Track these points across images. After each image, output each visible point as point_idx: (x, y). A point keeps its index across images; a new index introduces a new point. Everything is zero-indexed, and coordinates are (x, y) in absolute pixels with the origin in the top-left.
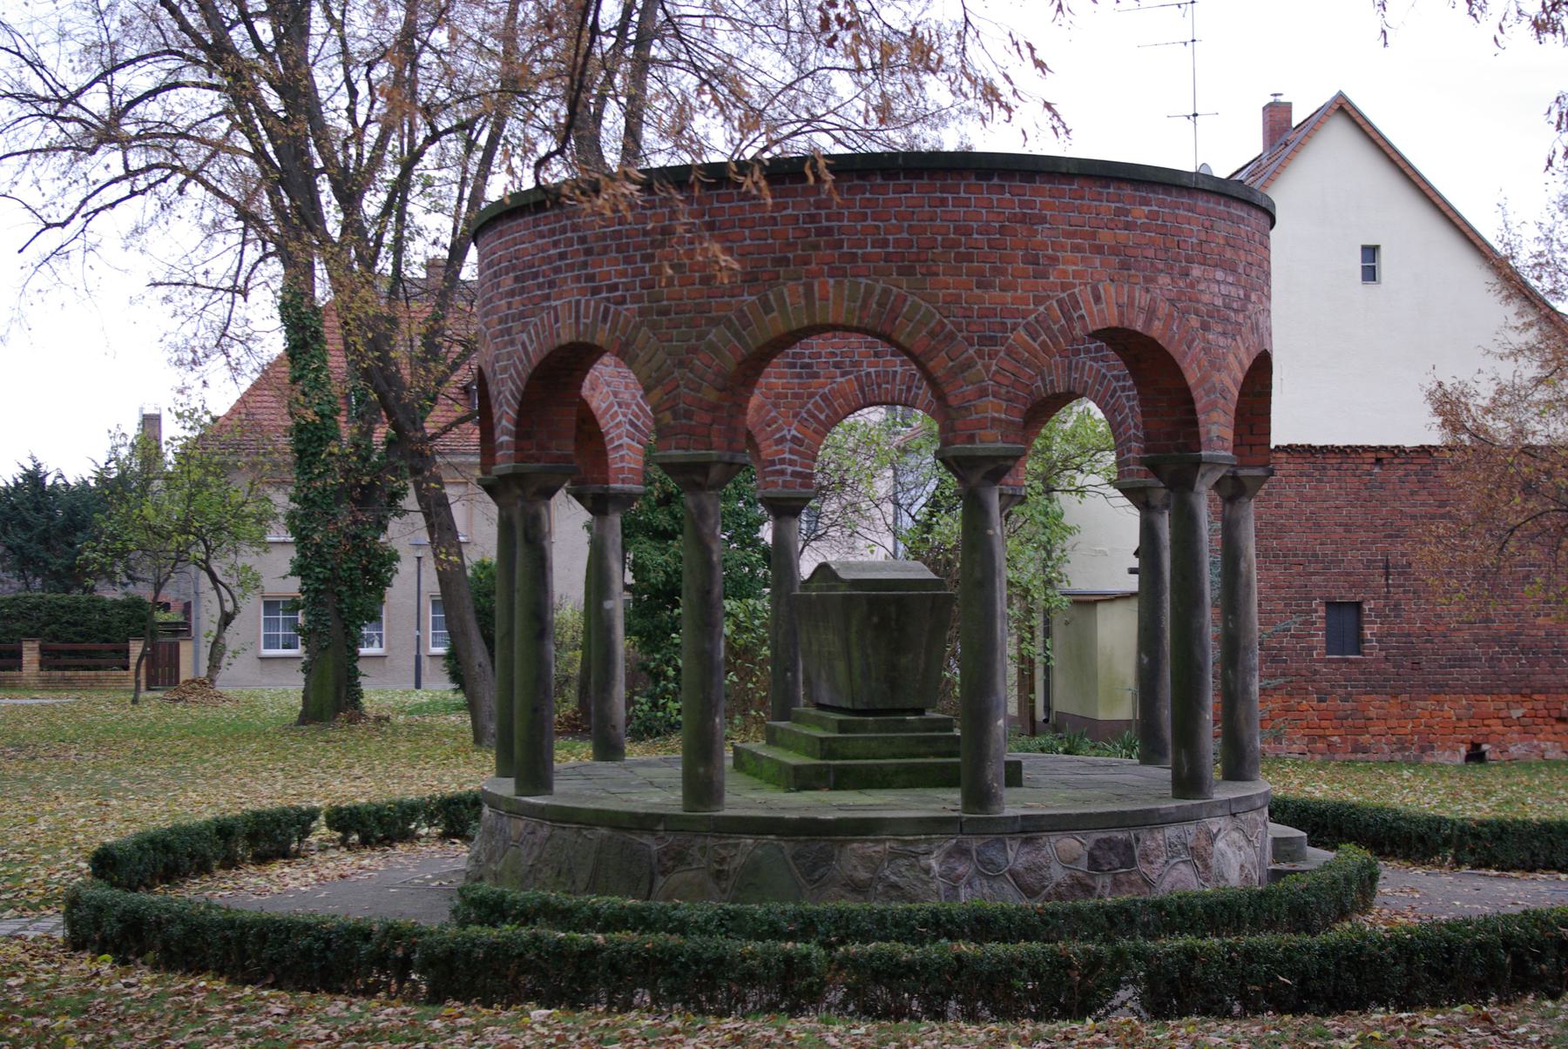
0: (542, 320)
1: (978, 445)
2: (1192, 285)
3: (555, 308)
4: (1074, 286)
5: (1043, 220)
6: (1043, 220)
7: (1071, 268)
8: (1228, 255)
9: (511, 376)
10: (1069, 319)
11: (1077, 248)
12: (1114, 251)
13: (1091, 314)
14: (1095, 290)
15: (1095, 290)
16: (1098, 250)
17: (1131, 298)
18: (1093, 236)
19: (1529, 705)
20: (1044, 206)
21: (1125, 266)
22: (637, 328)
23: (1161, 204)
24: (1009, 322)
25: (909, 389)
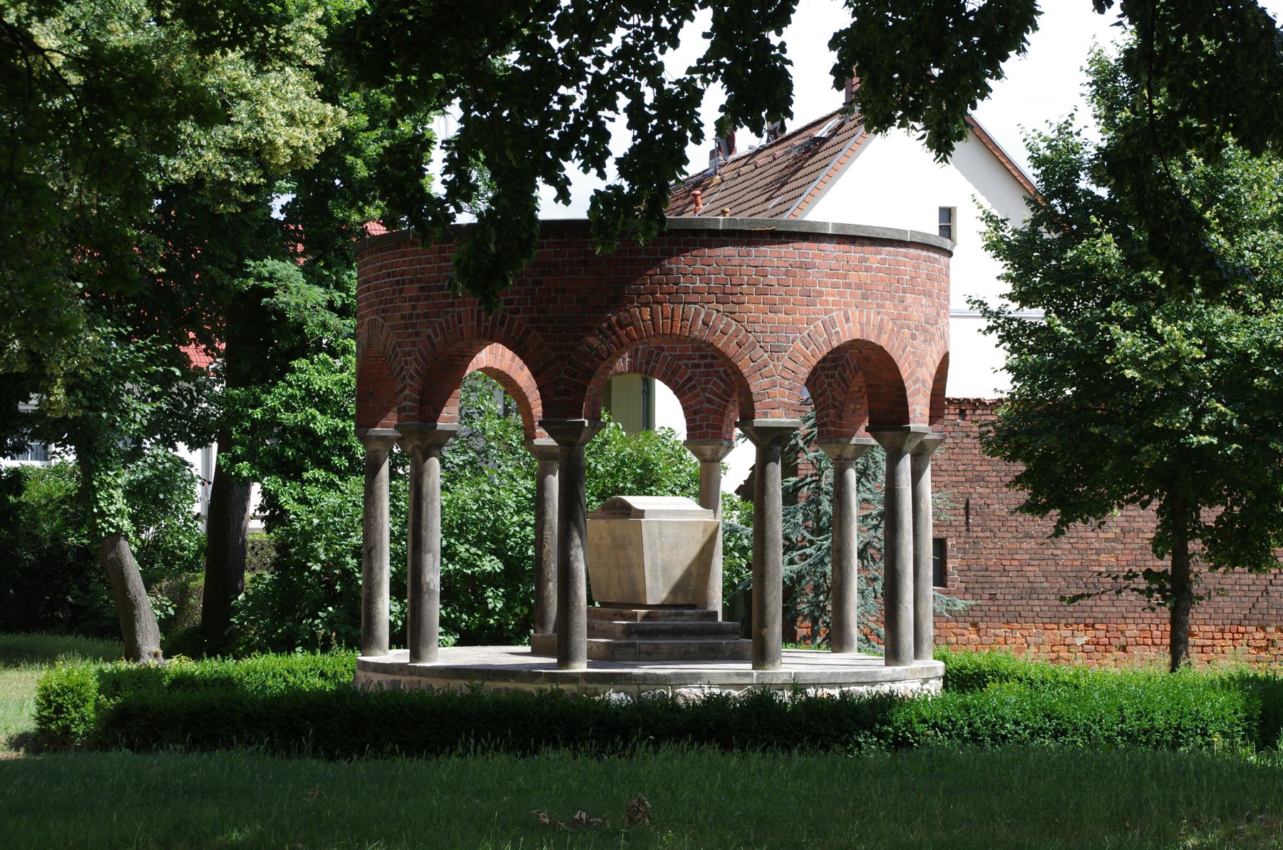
0: (446, 321)
1: (770, 420)
2: (906, 309)
3: (459, 314)
4: (832, 311)
5: (813, 266)
6: (813, 266)
7: (831, 299)
8: (928, 286)
9: (416, 359)
10: (829, 334)
11: (835, 286)
12: (859, 287)
13: (843, 330)
14: (846, 313)
15: (846, 313)
16: (848, 286)
17: (868, 318)
18: (845, 277)
19: (1091, 633)
20: (815, 256)
21: (865, 297)
22: (527, 332)
23: (889, 254)
24: (791, 336)
25: (648, 363)
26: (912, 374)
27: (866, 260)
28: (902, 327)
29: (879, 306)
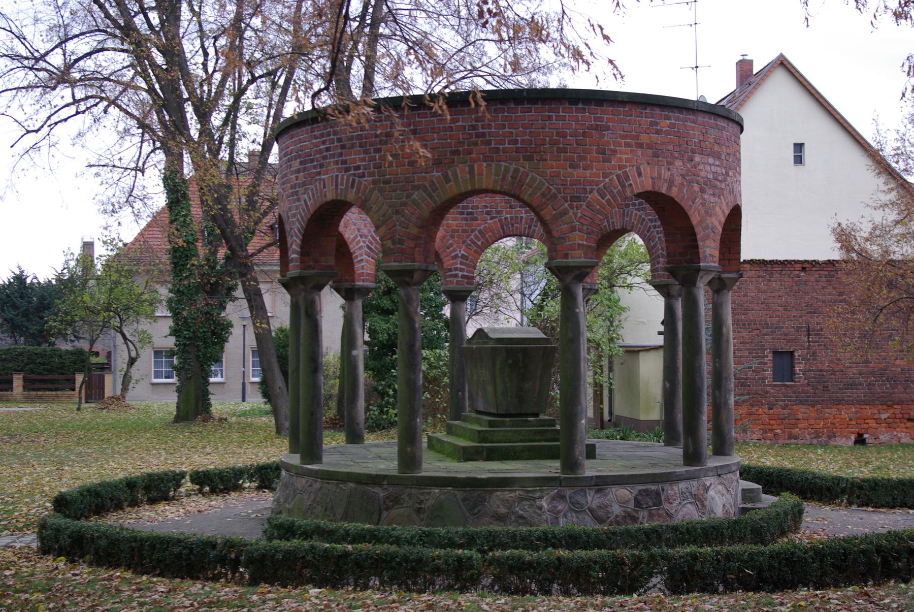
0: (316, 186)
1: (570, 260)
2: (695, 166)
3: (324, 180)
4: (626, 167)
5: (608, 128)
6: (608, 128)
7: (624, 156)
9: (298, 220)
10: (623, 186)
11: (628, 145)
12: (650, 146)
13: (636, 183)
14: (638, 169)
15: (638, 169)
16: (640, 146)
17: (659, 174)
19: (891, 411)
20: (609, 120)
21: (656, 155)
22: (371, 191)
23: (677, 119)
24: (588, 188)
25: (530, 227)
26: (701, 222)
27: (657, 124)
28: (691, 182)
29: (669, 163)
